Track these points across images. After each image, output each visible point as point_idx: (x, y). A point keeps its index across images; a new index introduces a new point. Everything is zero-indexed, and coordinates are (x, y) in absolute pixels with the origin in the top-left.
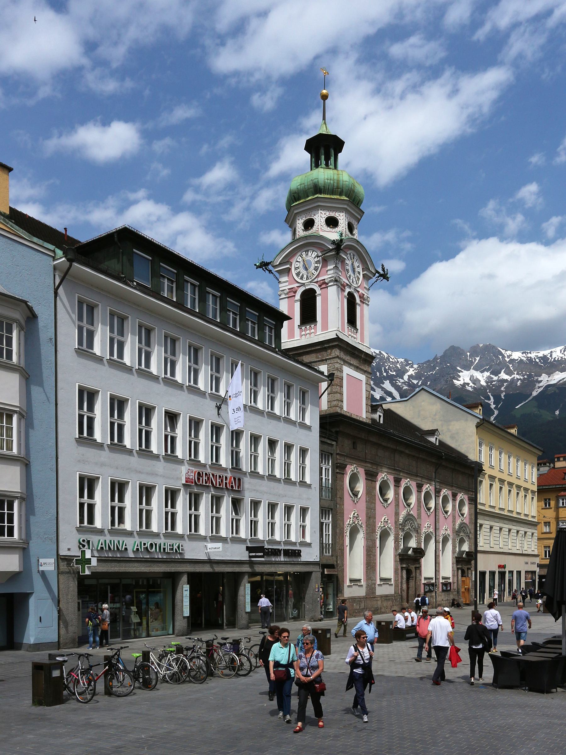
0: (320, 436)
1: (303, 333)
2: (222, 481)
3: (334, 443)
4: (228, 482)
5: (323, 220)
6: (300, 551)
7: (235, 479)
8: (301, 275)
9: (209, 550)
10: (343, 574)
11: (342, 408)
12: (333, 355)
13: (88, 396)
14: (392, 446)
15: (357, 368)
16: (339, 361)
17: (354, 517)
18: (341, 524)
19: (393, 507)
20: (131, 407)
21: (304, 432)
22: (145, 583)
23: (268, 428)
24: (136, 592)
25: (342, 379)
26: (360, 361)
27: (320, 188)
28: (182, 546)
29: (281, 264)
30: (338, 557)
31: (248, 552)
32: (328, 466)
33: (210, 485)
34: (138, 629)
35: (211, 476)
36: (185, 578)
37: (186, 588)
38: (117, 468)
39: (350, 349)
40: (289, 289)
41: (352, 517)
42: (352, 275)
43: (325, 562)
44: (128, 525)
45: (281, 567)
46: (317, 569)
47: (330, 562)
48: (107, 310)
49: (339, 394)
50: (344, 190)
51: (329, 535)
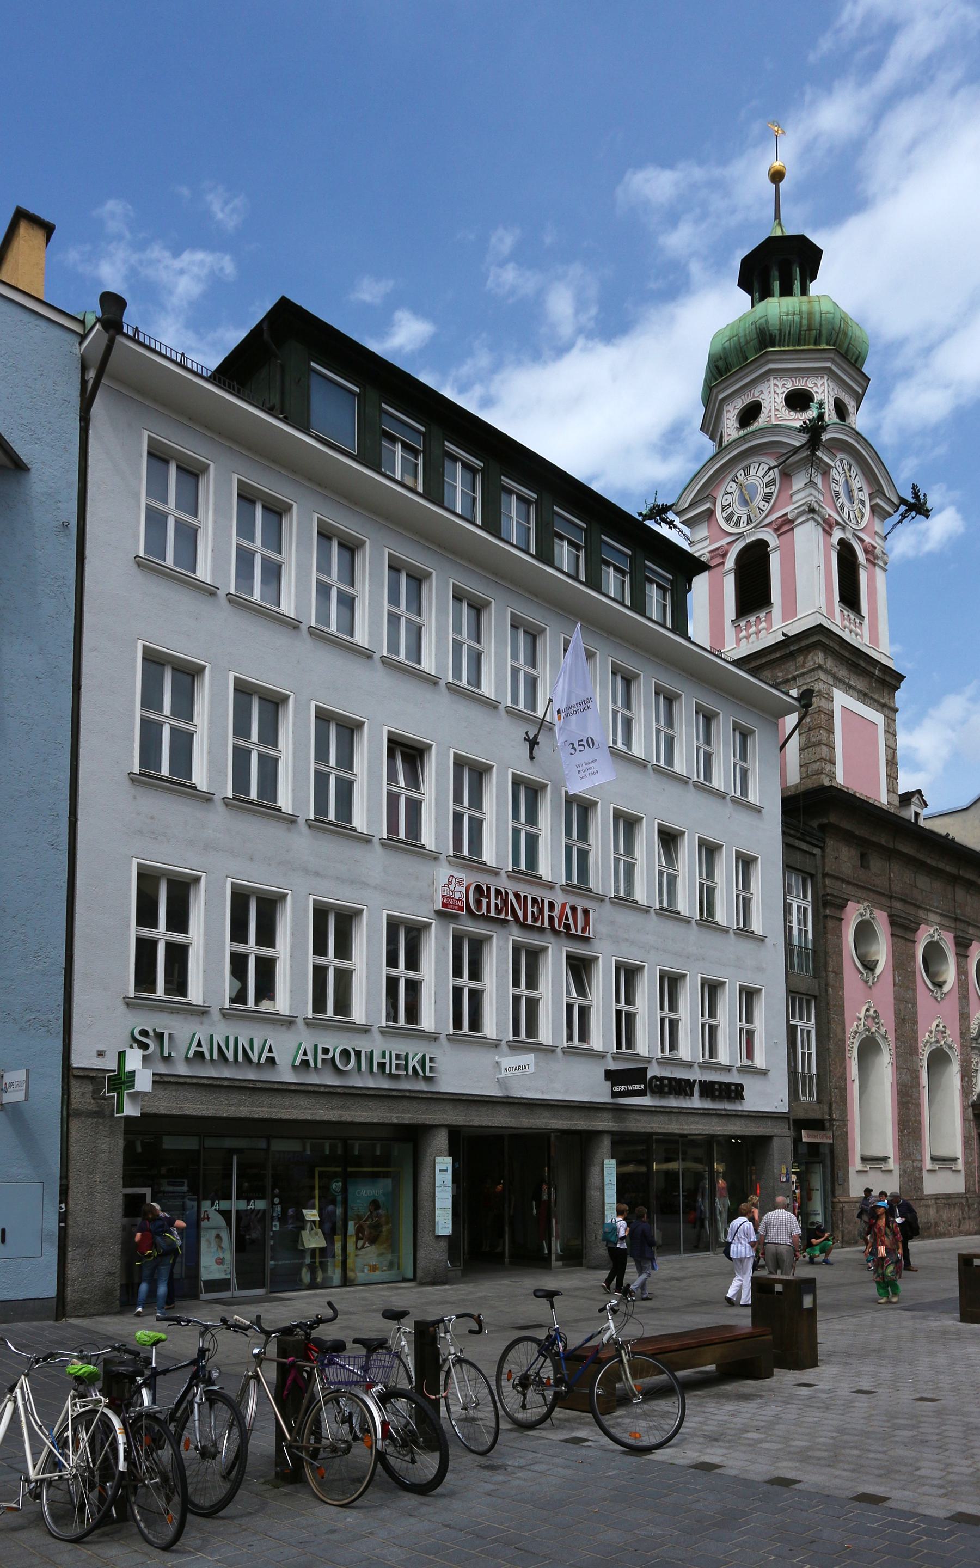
0: (783, 833)
1: (744, 633)
2: (541, 911)
3: (816, 851)
4: (556, 913)
5: (780, 399)
6: (742, 1086)
7: (574, 909)
8: (735, 518)
9: (504, 1074)
10: (846, 1144)
11: (833, 777)
12: (810, 665)
13: (170, 674)
14: (948, 869)
15: (864, 697)
16: (823, 676)
17: (867, 1017)
18: (839, 1030)
19: (954, 999)
20: (295, 716)
21: (744, 818)
22: (339, 1152)
23: (657, 806)
24: (322, 1175)
25: (831, 715)
26: (870, 684)
27: (771, 335)
28: (431, 1060)
29: (692, 505)
30: (834, 1105)
31: (609, 1083)
32: (802, 903)
33: (509, 918)
34: (323, 1266)
35: (511, 897)
36: (441, 1140)
37: (444, 1164)
38: (252, 859)
39: (847, 654)
40: (710, 552)
41: (862, 1016)
42: (847, 504)
43: (801, 1115)
44: (282, 1003)
45: (694, 1116)
46: (782, 1131)
47: (817, 1115)
48: (231, 480)
49: (824, 747)
50: (824, 332)
51: (810, 1055)
